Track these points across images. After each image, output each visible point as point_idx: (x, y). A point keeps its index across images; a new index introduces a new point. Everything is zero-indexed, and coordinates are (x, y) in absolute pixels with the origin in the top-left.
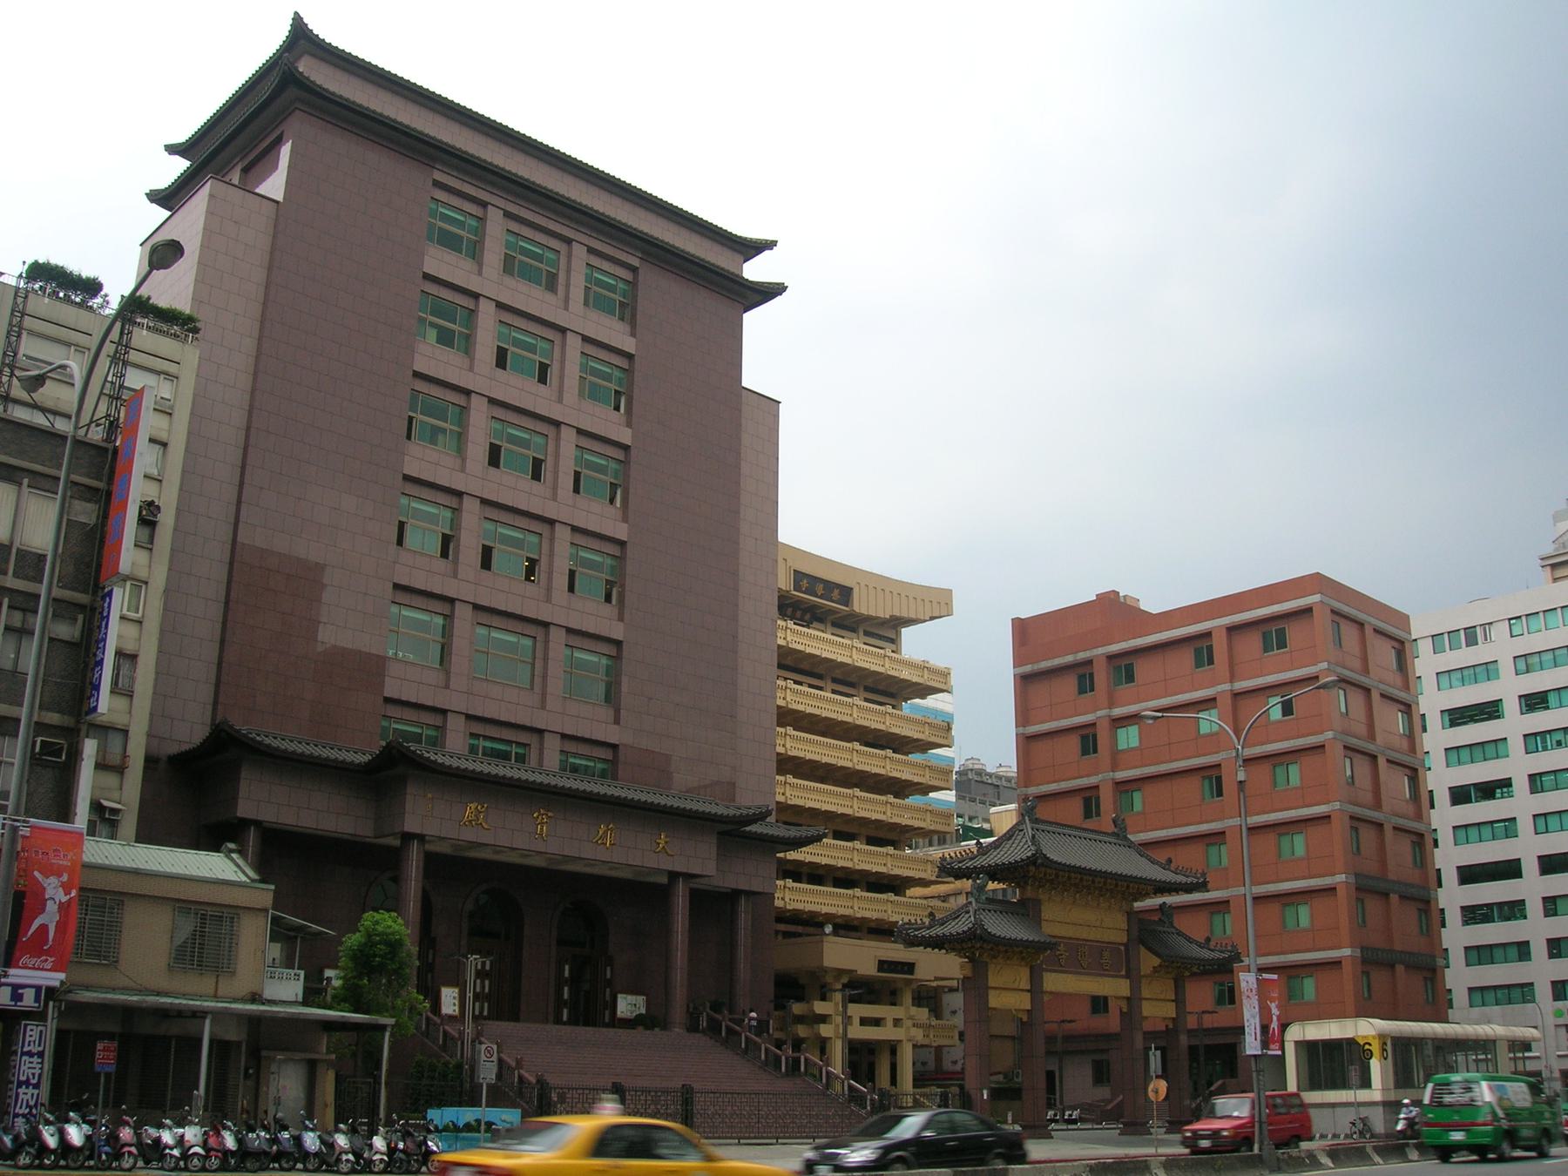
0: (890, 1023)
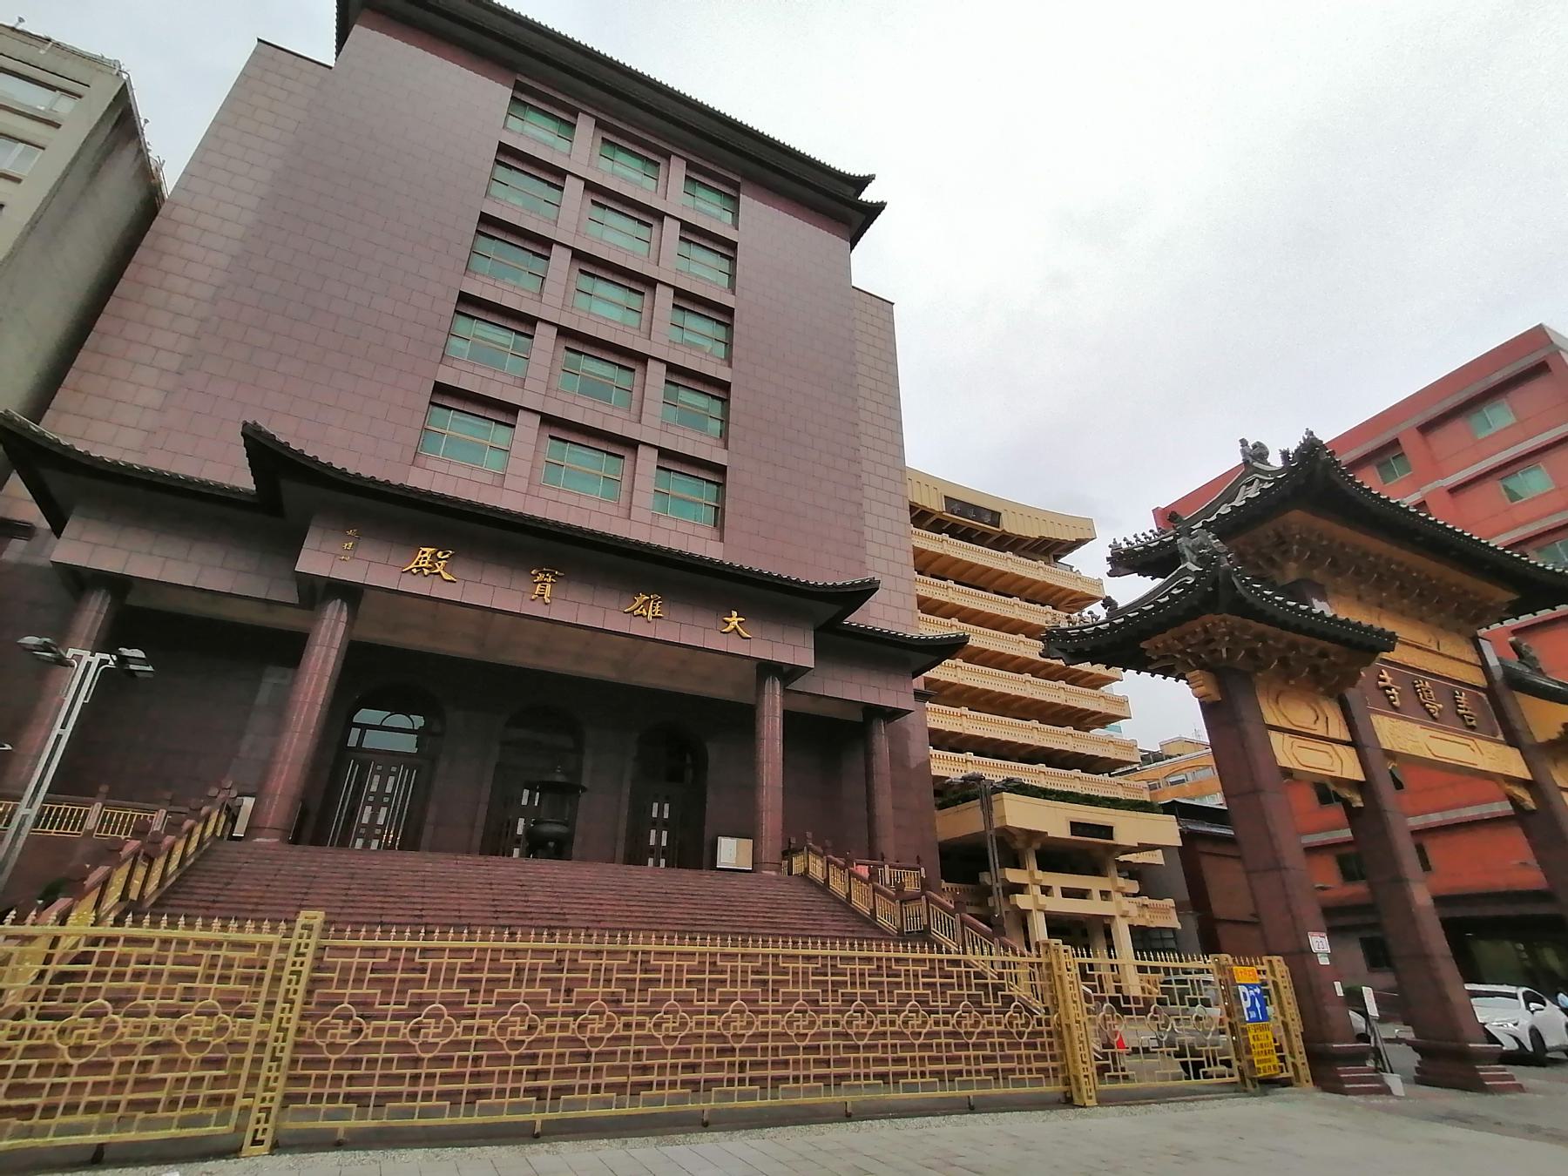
0: (1096, 894)
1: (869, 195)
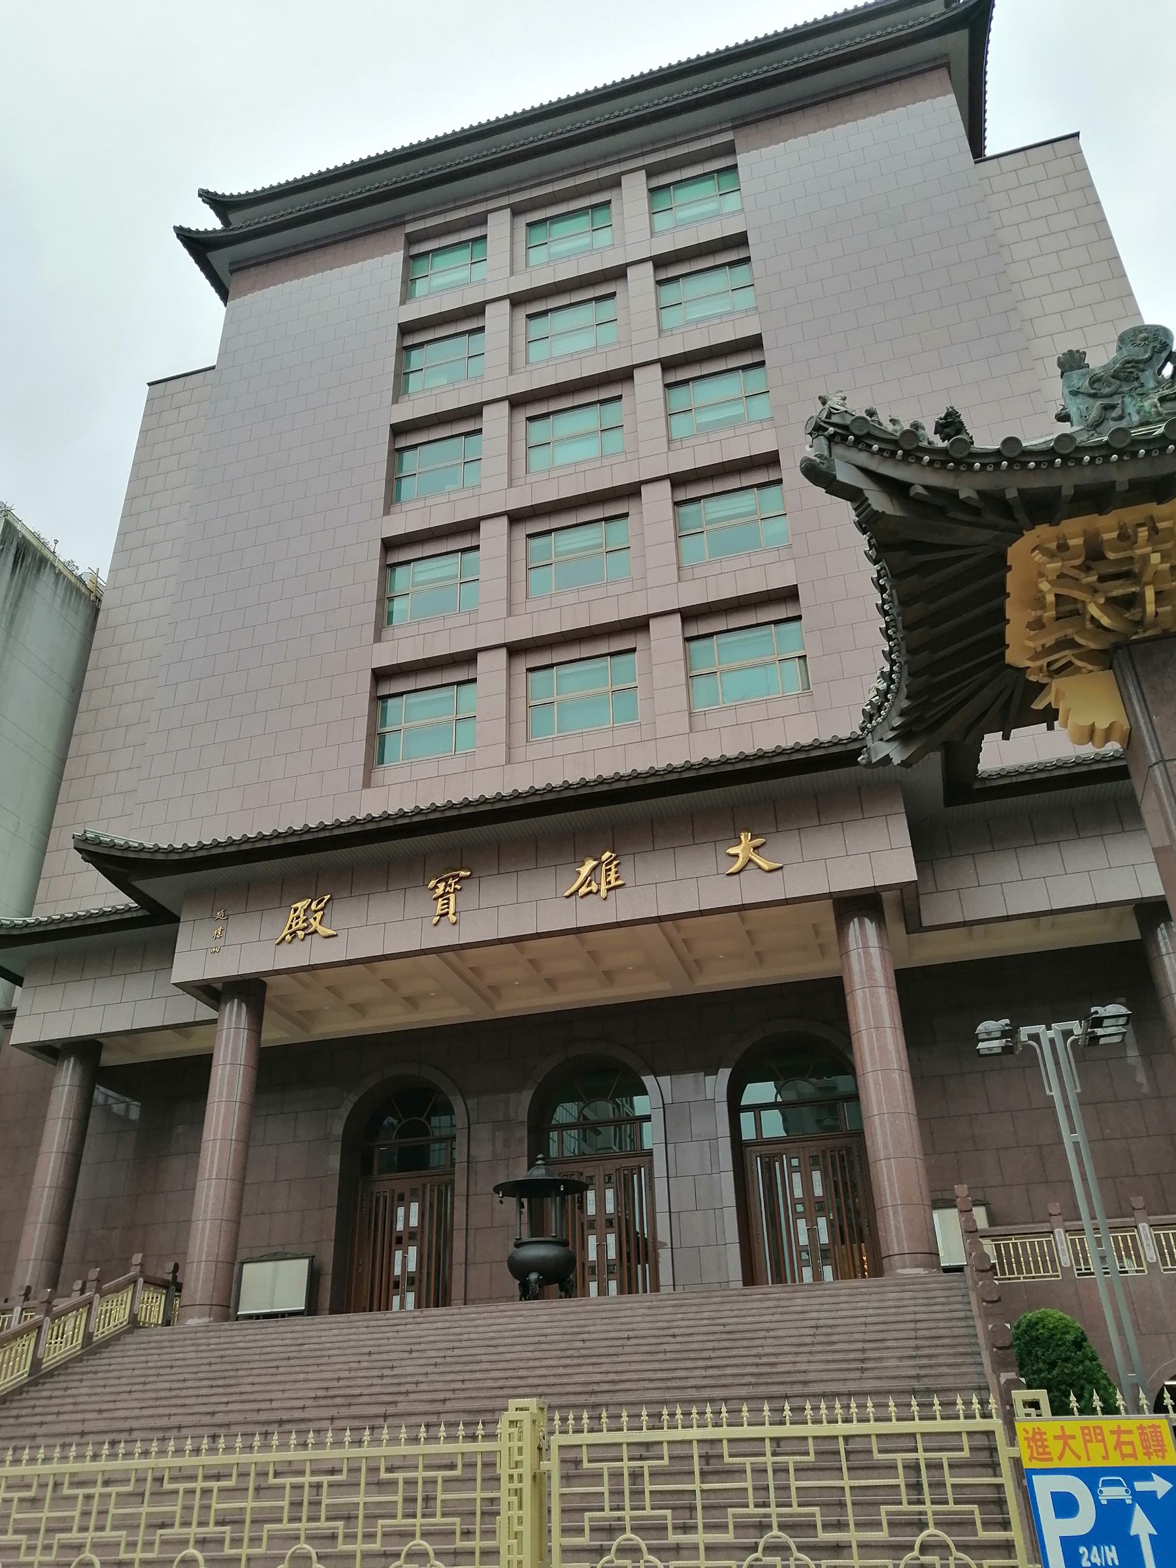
1: (207, 221)
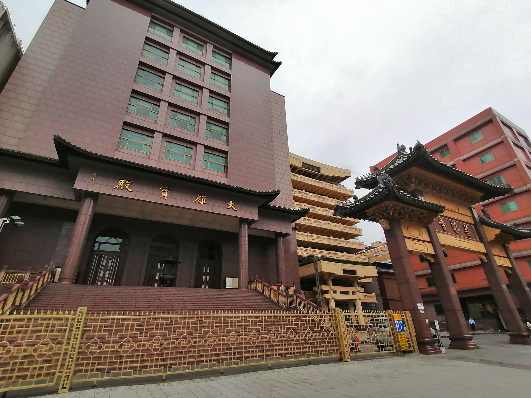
0: (351, 293)
